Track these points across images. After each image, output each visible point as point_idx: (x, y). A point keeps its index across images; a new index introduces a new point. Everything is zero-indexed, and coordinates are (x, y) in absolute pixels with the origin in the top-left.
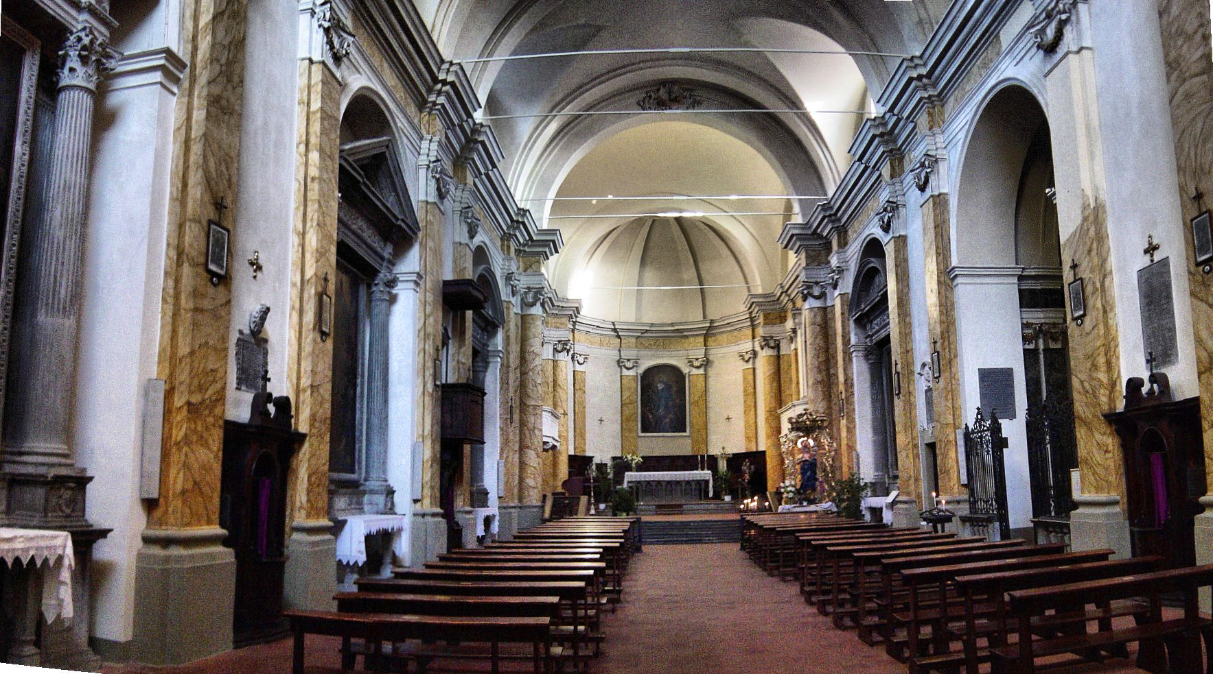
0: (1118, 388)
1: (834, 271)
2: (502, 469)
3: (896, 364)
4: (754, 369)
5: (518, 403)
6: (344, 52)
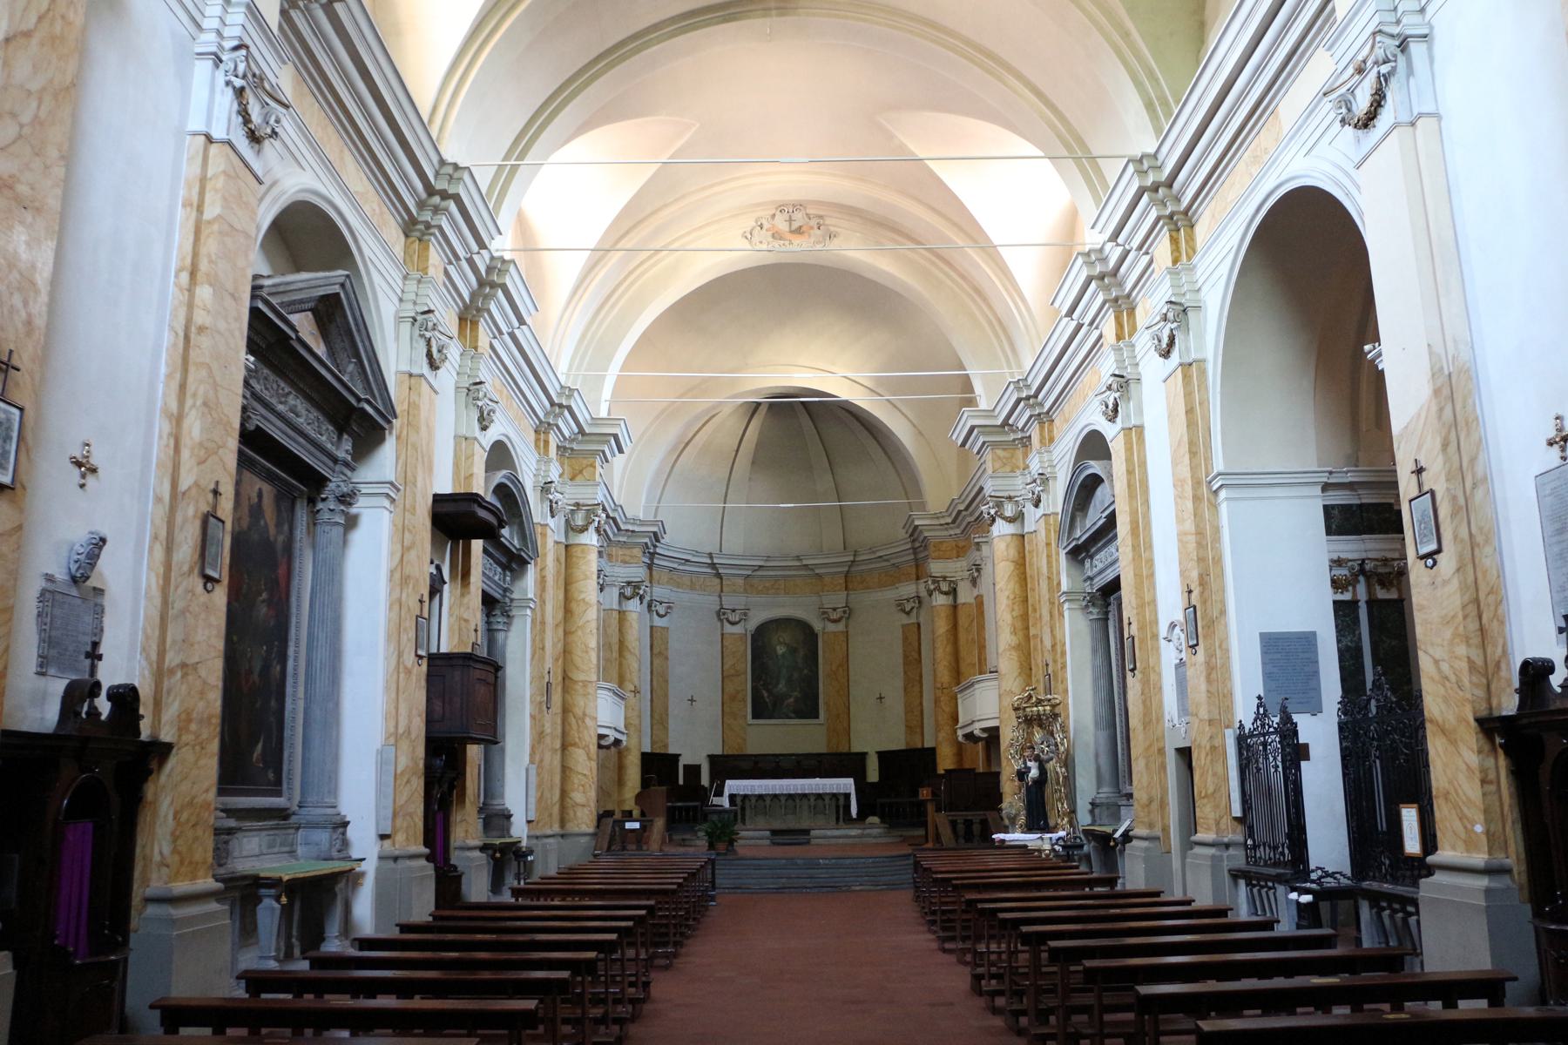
0: (1503, 673)
1: (1035, 481)
2: (533, 779)
3: (1130, 624)
4: (919, 625)
5: (560, 678)
6: (269, 131)
